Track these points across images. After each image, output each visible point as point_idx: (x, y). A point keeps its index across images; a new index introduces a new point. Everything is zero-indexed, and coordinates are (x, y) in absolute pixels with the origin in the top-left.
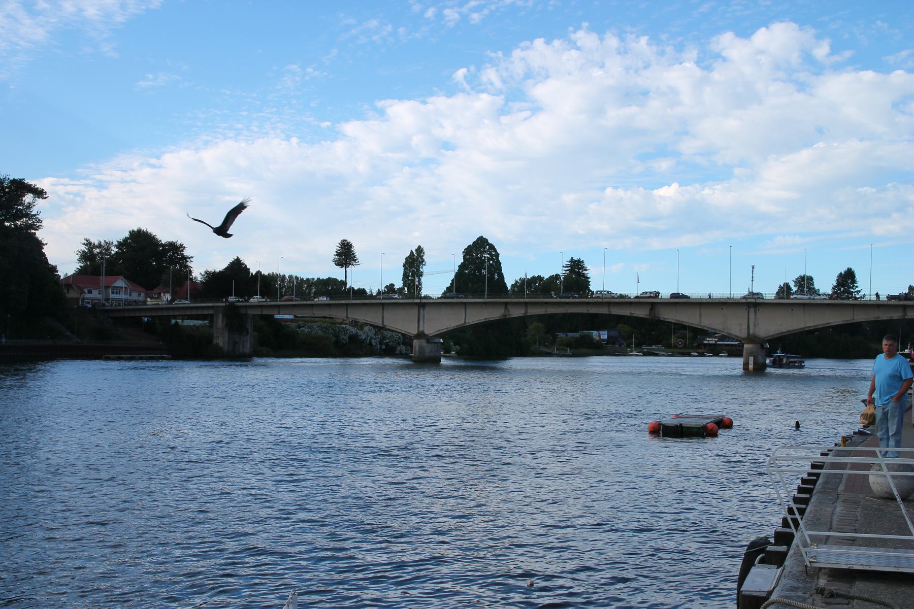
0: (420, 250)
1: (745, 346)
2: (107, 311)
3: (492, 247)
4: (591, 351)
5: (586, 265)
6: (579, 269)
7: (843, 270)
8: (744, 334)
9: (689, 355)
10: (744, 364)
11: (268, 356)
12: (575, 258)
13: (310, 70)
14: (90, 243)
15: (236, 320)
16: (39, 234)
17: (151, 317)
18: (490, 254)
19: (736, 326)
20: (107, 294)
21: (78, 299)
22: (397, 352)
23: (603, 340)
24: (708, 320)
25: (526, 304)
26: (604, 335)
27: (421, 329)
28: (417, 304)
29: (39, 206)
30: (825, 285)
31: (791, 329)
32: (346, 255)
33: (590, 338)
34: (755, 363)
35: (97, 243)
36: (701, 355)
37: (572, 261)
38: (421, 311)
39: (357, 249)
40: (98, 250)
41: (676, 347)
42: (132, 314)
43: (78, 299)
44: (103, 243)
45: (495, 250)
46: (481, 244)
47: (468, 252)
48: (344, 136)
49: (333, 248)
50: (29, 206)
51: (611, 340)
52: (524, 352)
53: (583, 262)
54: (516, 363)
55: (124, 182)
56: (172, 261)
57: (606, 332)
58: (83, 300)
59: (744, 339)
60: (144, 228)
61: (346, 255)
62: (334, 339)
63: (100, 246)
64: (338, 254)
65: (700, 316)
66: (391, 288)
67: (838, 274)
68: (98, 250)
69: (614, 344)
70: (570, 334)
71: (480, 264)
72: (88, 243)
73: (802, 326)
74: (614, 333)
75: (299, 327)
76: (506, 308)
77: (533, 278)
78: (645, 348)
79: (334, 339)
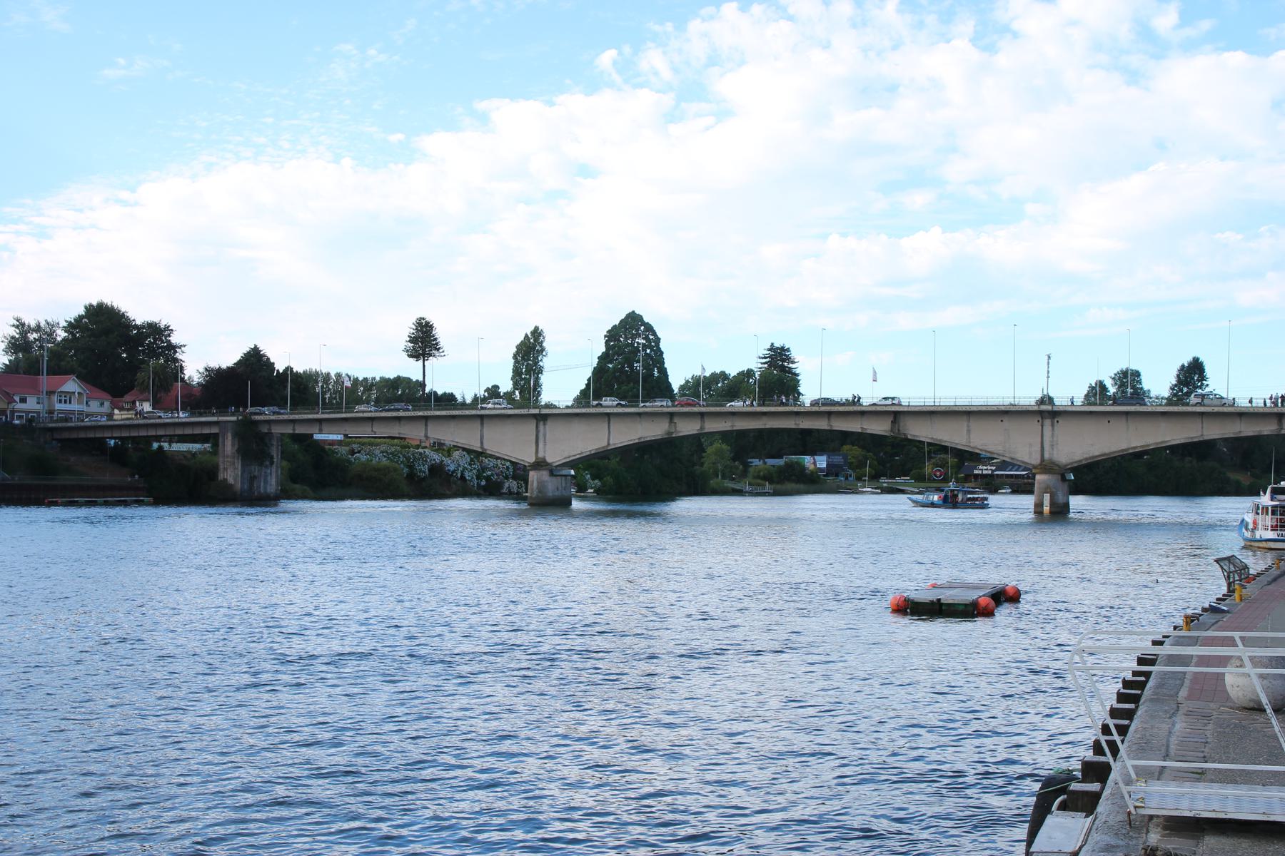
0: (537, 333)
1: (1038, 477)
2: (52, 430)
3: (649, 328)
4: (802, 486)
6: (783, 361)
7: (1186, 360)
8: (1035, 460)
12: (777, 345)
14: (23, 325)
15: (253, 444)
17: (121, 438)
18: (646, 338)
19: (1022, 446)
22: (504, 491)
23: (821, 470)
26: (822, 462)
27: (541, 455)
28: (534, 416)
30: (1159, 384)
31: (1107, 451)
32: (423, 342)
34: (1052, 504)
38: (541, 427)
39: (440, 333)
40: (35, 335)
41: (931, 480)
44: (43, 324)
45: (654, 333)
46: (633, 323)
47: (612, 335)
49: (406, 329)
51: (832, 470)
52: (698, 488)
53: (788, 350)
56: (153, 352)
57: (824, 458)
58: (13, 412)
59: (1035, 467)
61: (423, 342)
63: (38, 328)
64: (413, 340)
65: (969, 431)
66: (493, 392)
67: (1178, 367)
68: (35, 335)
69: (837, 475)
70: (770, 462)
72: (20, 325)
74: (838, 459)
75: (353, 453)
76: (671, 421)
78: (885, 482)
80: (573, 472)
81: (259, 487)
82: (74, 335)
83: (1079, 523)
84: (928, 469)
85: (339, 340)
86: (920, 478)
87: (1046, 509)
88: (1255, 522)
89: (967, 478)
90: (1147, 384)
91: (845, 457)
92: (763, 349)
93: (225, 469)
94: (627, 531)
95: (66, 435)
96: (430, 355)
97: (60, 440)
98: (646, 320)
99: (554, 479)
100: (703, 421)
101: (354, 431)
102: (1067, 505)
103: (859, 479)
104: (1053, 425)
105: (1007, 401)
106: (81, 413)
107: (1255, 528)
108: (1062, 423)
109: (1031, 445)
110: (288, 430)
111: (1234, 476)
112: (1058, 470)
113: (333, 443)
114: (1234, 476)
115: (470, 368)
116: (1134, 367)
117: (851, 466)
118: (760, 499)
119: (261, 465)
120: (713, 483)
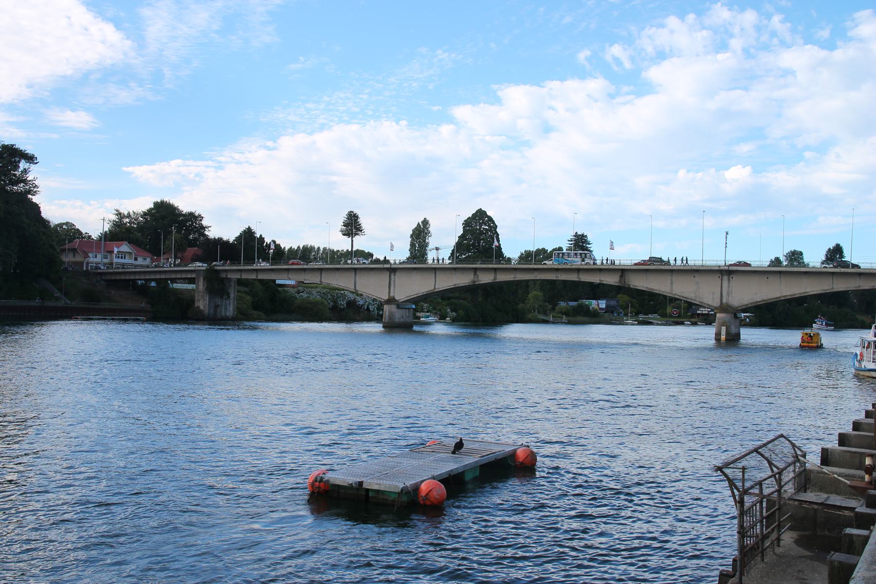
0: (425, 222)
1: (718, 315)
2: (100, 274)
3: (491, 219)
4: (586, 319)
5: (589, 239)
6: (583, 243)
7: (831, 246)
8: (716, 303)
9: (682, 323)
10: (716, 334)
11: (260, 319)
12: (579, 233)
13: (439, 52)
14: (120, 214)
15: (217, 285)
16: (35, 199)
17: (145, 280)
18: (489, 226)
19: (707, 294)
20: (112, 259)
21: (82, 263)
23: (601, 309)
24: (682, 289)
25: (495, 270)
26: (603, 304)
27: (392, 295)
28: (387, 269)
29: (34, 173)
30: (814, 258)
31: (766, 298)
32: (352, 226)
33: (588, 307)
34: (727, 333)
35: (126, 213)
36: (694, 324)
37: (576, 235)
38: (392, 277)
39: (363, 221)
40: (128, 220)
41: (671, 316)
42: (123, 277)
43: (82, 263)
44: (131, 213)
45: (493, 222)
46: (481, 215)
47: (467, 223)
48: (451, 120)
49: (341, 219)
50: (25, 171)
51: (609, 310)
52: (520, 318)
53: (586, 236)
54: (513, 331)
55: (238, 163)
56: (189, 230)
57: (604, 302)
58: (88, 263)
59: (716, 308)
60: (166, 199)
61: (352, 226)
62: (331, 304)
63: (129, 216)
65: (672, 283)
67: (827, 249)
68: (128, 220)
69: (612, 312)
70: (572, 304)
71: (479, 236)
72: (119, 214)
73: (778, 295)
74: (613, 303)
75: (299, 292)
76: (475, 274)
77: (538, 250)
78: (641, 317)
79: (331, 304)
80: (414, 306)
81: (221, 312)
82: (146, 219)
83: (745, 348)
84: (669, 310)
85: (297, 225)
86: (664, 315)
87: (723, 337)
88: (861, 355)
89: (693, 316)
90: (806, 259)
91: (618, 302)
92: (570, 235)
93: (199, 300)
94: (473, 346)
95: (109, 277)
96: (356, 234)
97: (105, 281)
98: (488, 214)
99: (400, 311)
100: (495, 274)
101: (302, 277)
102: (738, 336)
103: (626, 315)
104: (729, 280)
105: (699, 263)
106: (132, 265)
107: (862, 359)
108: (735, 279)
109: (713, 293)
110: (237, 276)
111: (860, 317)
112: (734, 312)
113: (288, 286)
114: (860, 317)
115: (387, 241)
116: (798, 249)
117: (622, 307)
118: (557, 326)
119: (222, 298)
120: (530, 316)
